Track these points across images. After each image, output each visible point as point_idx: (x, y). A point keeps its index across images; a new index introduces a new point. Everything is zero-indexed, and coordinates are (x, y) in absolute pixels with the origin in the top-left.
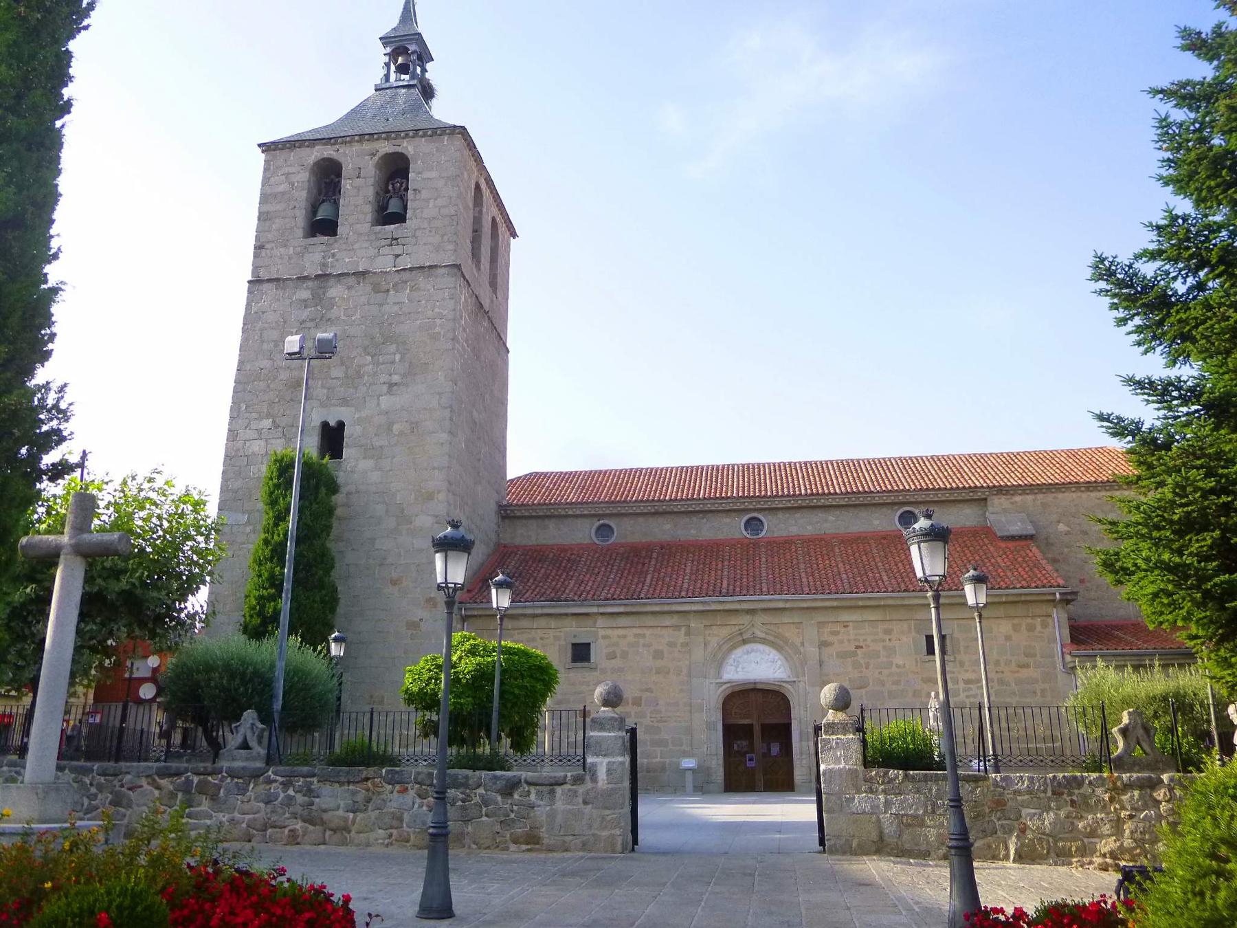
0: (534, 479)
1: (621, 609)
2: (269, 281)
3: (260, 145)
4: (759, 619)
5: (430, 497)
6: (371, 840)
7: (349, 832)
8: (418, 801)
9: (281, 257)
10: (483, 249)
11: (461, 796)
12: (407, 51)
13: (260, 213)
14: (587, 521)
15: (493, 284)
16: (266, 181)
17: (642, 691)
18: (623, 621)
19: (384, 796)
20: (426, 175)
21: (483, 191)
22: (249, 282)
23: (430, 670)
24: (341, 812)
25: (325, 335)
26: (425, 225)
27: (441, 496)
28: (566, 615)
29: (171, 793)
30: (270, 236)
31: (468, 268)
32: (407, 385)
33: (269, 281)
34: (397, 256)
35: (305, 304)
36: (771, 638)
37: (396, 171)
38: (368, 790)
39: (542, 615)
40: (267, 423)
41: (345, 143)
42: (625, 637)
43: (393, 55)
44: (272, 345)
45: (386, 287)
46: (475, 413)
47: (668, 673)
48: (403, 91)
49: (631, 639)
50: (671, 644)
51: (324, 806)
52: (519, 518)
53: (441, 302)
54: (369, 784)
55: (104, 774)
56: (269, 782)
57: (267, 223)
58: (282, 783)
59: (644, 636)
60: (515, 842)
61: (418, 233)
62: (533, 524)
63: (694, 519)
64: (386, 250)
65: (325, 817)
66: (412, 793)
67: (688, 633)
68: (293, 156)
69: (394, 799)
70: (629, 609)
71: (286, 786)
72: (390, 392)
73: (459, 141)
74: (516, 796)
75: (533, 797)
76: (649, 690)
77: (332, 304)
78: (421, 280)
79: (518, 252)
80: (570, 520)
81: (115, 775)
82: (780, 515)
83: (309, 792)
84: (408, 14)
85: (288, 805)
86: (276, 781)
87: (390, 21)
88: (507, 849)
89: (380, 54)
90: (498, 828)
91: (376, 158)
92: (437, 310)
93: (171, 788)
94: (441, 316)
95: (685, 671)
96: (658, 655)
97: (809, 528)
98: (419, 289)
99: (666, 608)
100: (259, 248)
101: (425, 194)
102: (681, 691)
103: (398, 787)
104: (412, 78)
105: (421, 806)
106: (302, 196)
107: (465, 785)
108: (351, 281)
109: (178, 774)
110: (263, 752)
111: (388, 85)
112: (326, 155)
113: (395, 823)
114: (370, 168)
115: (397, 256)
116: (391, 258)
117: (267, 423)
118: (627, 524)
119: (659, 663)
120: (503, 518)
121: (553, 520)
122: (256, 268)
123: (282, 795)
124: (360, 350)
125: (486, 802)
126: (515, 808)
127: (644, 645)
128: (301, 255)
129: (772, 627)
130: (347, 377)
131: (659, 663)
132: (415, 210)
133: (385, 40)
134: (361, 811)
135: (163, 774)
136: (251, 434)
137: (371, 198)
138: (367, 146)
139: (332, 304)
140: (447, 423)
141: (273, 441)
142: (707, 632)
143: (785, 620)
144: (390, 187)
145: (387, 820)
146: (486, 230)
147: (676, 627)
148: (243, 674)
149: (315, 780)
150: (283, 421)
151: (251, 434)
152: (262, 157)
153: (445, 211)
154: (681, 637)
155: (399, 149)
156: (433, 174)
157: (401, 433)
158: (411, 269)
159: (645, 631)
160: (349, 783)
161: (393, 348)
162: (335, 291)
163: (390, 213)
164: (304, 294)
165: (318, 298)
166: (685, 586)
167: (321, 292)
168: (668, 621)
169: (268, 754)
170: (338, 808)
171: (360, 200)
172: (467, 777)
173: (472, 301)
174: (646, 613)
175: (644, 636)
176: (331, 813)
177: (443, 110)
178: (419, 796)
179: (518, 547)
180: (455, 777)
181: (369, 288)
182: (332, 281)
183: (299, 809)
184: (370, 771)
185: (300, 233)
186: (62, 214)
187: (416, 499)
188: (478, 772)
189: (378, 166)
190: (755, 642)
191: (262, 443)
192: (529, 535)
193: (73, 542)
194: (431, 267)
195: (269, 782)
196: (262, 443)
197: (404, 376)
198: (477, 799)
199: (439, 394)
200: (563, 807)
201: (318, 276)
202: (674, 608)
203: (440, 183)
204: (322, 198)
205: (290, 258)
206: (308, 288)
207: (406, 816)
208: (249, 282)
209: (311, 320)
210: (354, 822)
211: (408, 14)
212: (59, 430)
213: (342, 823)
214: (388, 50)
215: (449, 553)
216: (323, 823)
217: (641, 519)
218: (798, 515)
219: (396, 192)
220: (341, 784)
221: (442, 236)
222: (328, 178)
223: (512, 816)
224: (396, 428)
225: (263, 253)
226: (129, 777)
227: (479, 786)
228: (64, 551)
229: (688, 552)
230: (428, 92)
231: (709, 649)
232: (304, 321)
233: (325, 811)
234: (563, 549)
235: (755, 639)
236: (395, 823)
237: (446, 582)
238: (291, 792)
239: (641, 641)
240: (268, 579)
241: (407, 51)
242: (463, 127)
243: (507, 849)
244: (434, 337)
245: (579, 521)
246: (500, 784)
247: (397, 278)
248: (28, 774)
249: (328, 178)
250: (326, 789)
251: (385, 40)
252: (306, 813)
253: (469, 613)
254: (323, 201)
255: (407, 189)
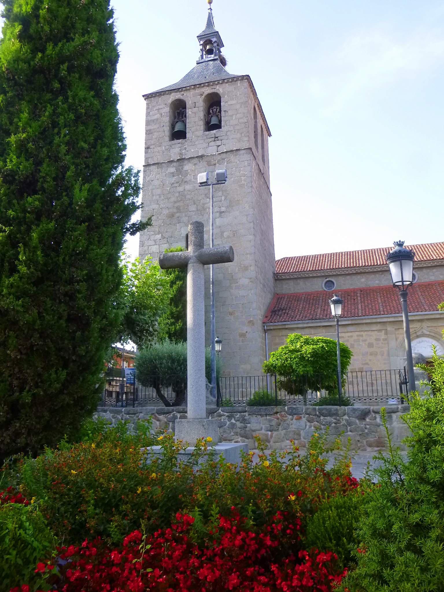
0: (287, 260)
1: (349, 322)
2: (154, 164)
3: (143, 96)
4: (425, 324)
5: (246, 268)
6: (283, 446)
7: (269, 442)
8: (308, 424)
9: (158, 152)
10: (258, 142)
11: (334, 421)
12: (211, 43)
13: (147, 131)
14: (320, 279)
15: (264, 161)
16: (148, 114)
17: (363, 364)
18: (350, 328)
19: (287, 422)
20: (230, 103)
21: (257, 110)
22: (144, 166)
23: (286, 354)
24: (263, 431)
25: (220, 171)
26: (232, 128)
27: (252, 268)
28: (320, 326)
29: (166, 423)
30: (152, 142)
31: (254, 149)
32: (229, 212)
33: (154, 164)
34: (218, 146)
35: (173, 175)
36: (433, 334)
37: (214, 103)
38: (278, 419)
39: (306, 327)
40: (159, 236)
41: (187, 90)
42: (352, 336)
43: (204, 45)
44: (158, 197)
45: (214, 162)
46: (262, 226)
47: (376, 355)
48: (211, 62)
49: (356, 338)
50: (377, 340)
51: (253, 428)
52: (283, 279)
53: (240, 169)
54: (278, 415)
55: (128, 414)
56: (220, 416)
57: (150, 135)
58: (228, 416)
59: (362, 336)
60: (370, 446)
61: (228, 133)
62: (291, 283)
63: (377, 275)
64: (212, 144)
65: (254, 434)
66: (304, 419)
67: (386, 333)
68: (160, 99)
69: (294, 424)
70: (353, 322)
71: (230, 417)
72: (220, 216)
73: (246, 83)
74: (367, 420)
75: (378, 420)
76: (367, 364)
77: (186, 173)
78: (232, 157)
79: (272, 143)
80: (311, 279)
81: (135, 414)
82: (425, 271)
83: (243, 420)
84: (210, 23)
85: (232, 428)
86: (224, 415)
87: (201, 28)
88: (365, 450)
89: (196, 47)
90: (358, 438)
91: (203, 96)
92: (242, 172)
93: (166, 420)
94: (244, 175)
95: (386, 354)
96: (370, 345)
97: (442, 277)
98: (231, 162)
99: (374, 321)
100: (147, 148)
101: (230, 113)
102: (385, 364)
103: (295, 416)
104: (215, 56)
105: (310, 427)
106: (166, 120)
107: (336, 414)
108: (196, 161)
109: (169, 413)
110: (215, 400)
111: (203, 60)
112: (177, 97)
113: (296, 437)
114: (201, 103)
115: (218, 146)
116: (215, 147)
117: (159, 236)
118: (341, 278)
119: (371, 350)
120: (276, 280)
121: (302, 280)
122: (146, 159)
123: (228, 423)
124: (203, 196)
125: (349, 424)
126: (368, 426)
127: (363, 341)
128: (168, 150)
129: (433, 328)
130: (198, 210)
131: (371, 350)
132: (226, 121)
133: (200, 37)
134: (275, 431)
135: (160, 412)
136: (151, 242)
137: (202, 117)
138: (198, 91)
139: (186, 173)
140: (252, 229)
141: (163, 245)
142: (397, 332)
143: (440, 324)
144: (211, 111)
145: (291, 435)
146: (260, 130)
147: (380, 331)
148: (179, 361)
149: (247, 414)
150: (166, 235)
151: (151, 242)
152: (143, 103)
153: (241, 121)
154: (382, 335)
155: (213, 91)
156: (234, 102)
157: (228, 237)
158: (226, 152)
159: (362, 333)
160: (266, 415)
161: (220, 193)
162: (188, 167)
163: (212, 124)
164: (172, 170)
165: (179, 171)
166: (381, 309)
167: (180, 168)
168: (374, 328)
169: (218, 401)
170: (261, 429)
171: (196, 119)
172: (337, 410)
173: (257, 167)
174: (363, 324)
175: (362, 336)
176: (257, 432)
177: (233, 69)
178: (309, 421)
179: (285, 295)
180: (330, 410)
181: (205, 164)
182: (186, 162)
183: (238, 430)
184: (279, 408)
185: (167, 138)
186: (117, 76)
187: (239, 270)
188: (342, 407)
189: (205, 101)
190: (423, 336)
191: (157, 246)
192: (290, 288)
193: (196, 254)
194: (237, 150)
195: (220, 416)
196: (157, 246)
197: (227, 207)
198: (344, 422)
199: (247, 215)
200: (397, 426)
201: (178, 160)
202: (378, 320)
203: (238, 106)
204: (176, 120)
205: (163, 152)
206: (173, 167)
207: (302, 433)
208: (144, 166)
209: (177, 183)
210: (272, 436)
211: (210, 23)
212: (134, 203)
213: (264, 437)
214: (202, 42)
215: (403, 261)
216: (253, 438)
217: (348, 277)
218: (434, 270)
219: (215, 114)
220: (262, 415)
221: (241, 134)
222: (179, 110)
223: (366, 431)
224: (226, 234)
225: (149, 150)
226: (141, 415)
227: (344, 415)
228: (191, 261)
229: (377, 293)
230: (223, 62)
231: (399, 340)
232: (173, 183)
233: (254, 431)
234: (309, 294)
235: (424, 335)
236: (296, 437)
237: (403, 281)
238: (233, 421)
239: (361, 338)
240: (170, 314)
241: (211, 43)
242: (248, 76)
243: (365, 450)
244: (242, 186)
245: (316, 279)
246: (357, 413)
247: (219, 158)
248: (190, 414)
249: (179, 110)
250: (253, 419)
251: (200, 37)
252: (243, 432)
253: (268, 328)
254: (177, 122)
255: (220, 112)
